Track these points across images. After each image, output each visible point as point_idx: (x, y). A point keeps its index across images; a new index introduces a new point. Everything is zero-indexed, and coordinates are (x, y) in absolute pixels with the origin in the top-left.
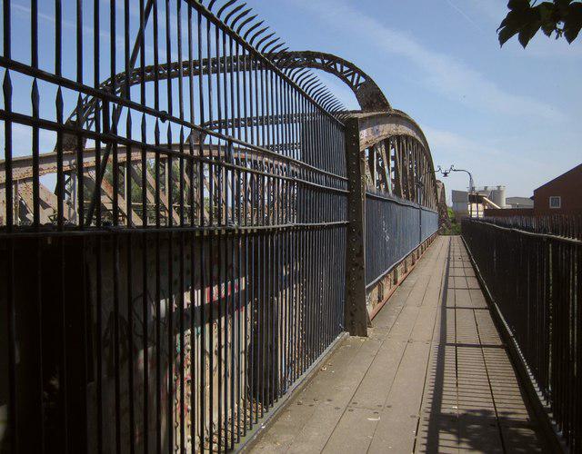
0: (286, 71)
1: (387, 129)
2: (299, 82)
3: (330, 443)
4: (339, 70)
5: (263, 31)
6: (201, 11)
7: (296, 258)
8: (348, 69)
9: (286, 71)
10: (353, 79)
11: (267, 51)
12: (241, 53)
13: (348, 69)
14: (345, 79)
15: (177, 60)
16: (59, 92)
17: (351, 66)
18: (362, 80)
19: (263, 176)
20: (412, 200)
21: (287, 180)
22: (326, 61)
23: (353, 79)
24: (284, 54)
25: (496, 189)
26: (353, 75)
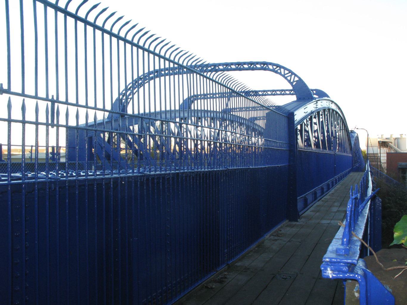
0: (251, 98)
1: (311, 107)
2: (263, 103)
3: (286, 265)
4: (283, 73)
5: (245, 88)
6: (57, 8)
7: (249, 163)
8: (276, 67)
9: (251, 98)
10: (287, 74)
11: (189, 64)
12: (258, 106)
13: (276, 67)
14: (286, 78)
15: (184, 75)
16: (87, 110)
17: (290, 71)
18: (296, 79)
19: (227, 144)
20: (345, 152)
21: (248, 146)
22: (225, 66)
23: (287, 74)
24: (202, 66)
25: (399, 137)
26: (291, 76)
